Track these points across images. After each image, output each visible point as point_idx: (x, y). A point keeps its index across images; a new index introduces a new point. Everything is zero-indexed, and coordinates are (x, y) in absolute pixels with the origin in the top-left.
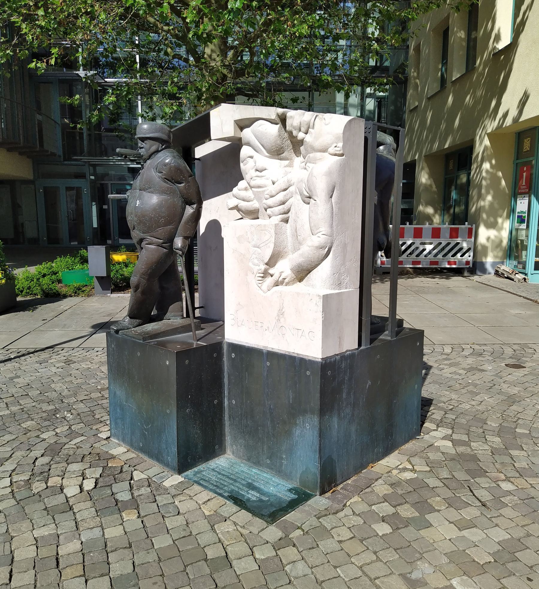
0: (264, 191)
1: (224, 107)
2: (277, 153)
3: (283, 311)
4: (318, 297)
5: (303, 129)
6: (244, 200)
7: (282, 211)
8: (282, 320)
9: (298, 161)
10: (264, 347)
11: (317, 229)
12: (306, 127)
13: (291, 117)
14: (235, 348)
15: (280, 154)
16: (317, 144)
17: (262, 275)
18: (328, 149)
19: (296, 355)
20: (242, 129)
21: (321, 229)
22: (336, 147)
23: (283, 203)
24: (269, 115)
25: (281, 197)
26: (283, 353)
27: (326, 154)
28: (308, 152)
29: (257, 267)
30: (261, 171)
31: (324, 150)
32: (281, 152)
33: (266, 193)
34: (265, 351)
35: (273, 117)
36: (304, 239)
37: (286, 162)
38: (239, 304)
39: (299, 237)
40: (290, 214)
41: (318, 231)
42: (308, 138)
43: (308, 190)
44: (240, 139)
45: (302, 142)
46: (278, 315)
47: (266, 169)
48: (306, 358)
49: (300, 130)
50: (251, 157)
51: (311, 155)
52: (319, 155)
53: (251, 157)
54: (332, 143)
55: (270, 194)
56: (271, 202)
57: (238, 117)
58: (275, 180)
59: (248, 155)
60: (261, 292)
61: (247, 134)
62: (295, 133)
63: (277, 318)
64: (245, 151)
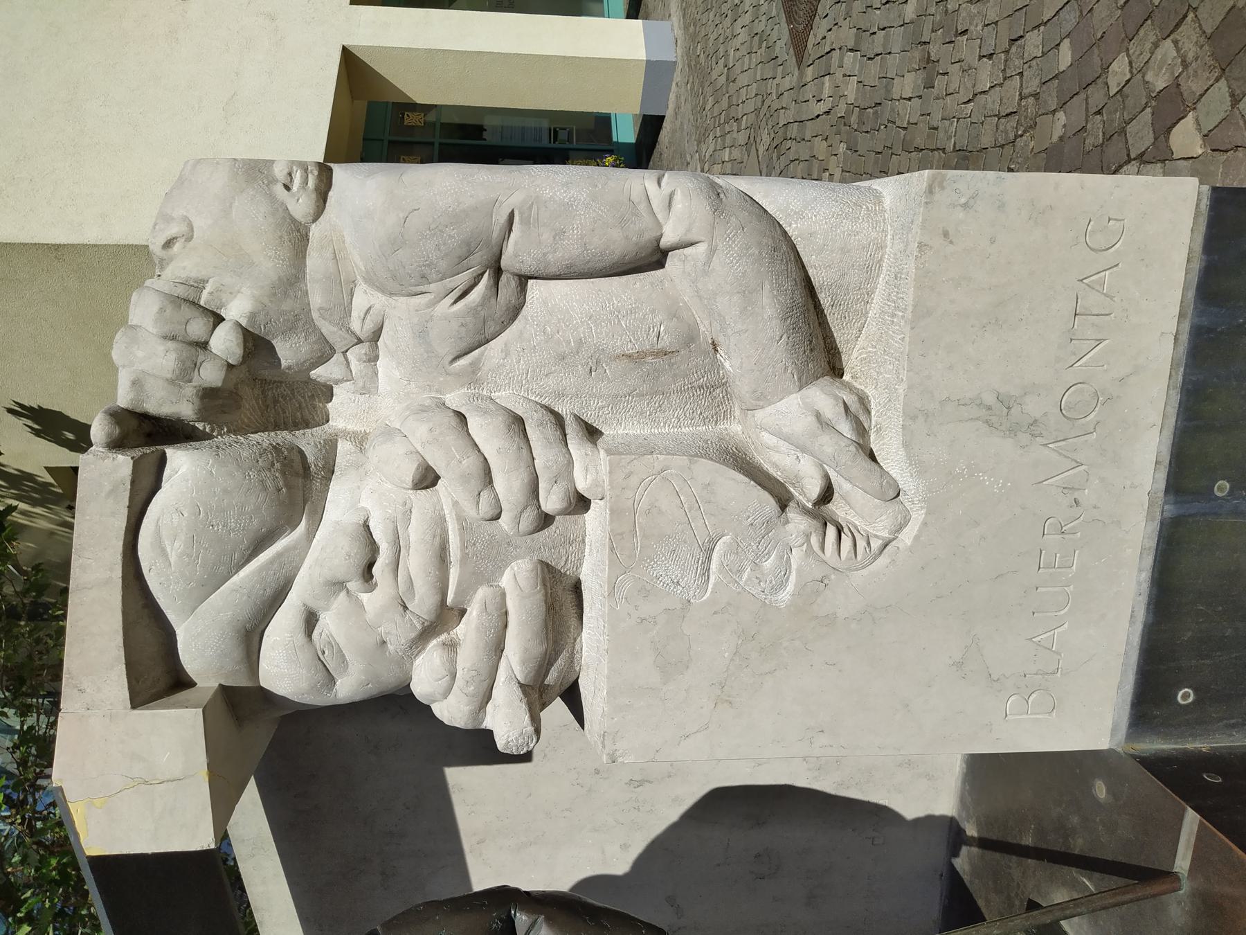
0: (461, 519)
1: (67, 772)
2: (298, 486)
3: (989, 399)
4: (938, 196)
5: (197, 328)
6: (498, 648)
7: (552, 432)
8: (1034, 407)
9: (343, 412)
10: (1149, 517)
11: (636, 213)
12: (187, 311)
13: (136, 384)
14: (1149, 699)
15: (306, 467)
16: (268, 263)
17: (831, 531)
18: (293, 220)
19: (1186, 326)
20: (178, 682)
21: (636, 194)
22: (287, 188)
23: (518, 422)
24: (113, 491)
25: (488, 434)
26: (1176, 397)
27: (315, 231)
28: (300, 321)
29: (796, 557)
30: (373, 549)
31: (298, 237)
32: (297, 459)
33: (470, 511)
34: (1170, 510)
35: (122, 464)
36: (674, 314)
37: (343, 447)
38: (959, 665)
39: (666, 341)
40: (563, 409)
41: (642, 207)
42: (237, 310)
43: (464, 278)
44: (228, 694)
45: (256, 345)
46: (1012, 431)
47: (366, 527)
48: (1196, 266)
49: (204, 345)
50: (310, 620)
51: (316, 299)
52: (314, 262)
53: (310, 620)
54: (272, 198)
55: (475, 484)
56: (508, 485)
57: (116, 685)
58: (409, 471)
59: (300, 637)
60: (907, 537)
61: (200, 646)
62: (211, 375)
63: (1024, 438)
64: (282, 671)
